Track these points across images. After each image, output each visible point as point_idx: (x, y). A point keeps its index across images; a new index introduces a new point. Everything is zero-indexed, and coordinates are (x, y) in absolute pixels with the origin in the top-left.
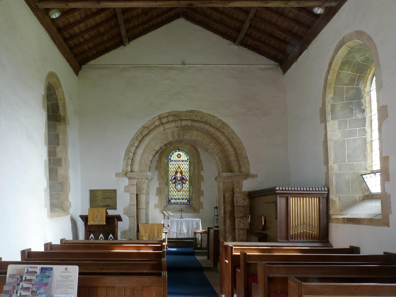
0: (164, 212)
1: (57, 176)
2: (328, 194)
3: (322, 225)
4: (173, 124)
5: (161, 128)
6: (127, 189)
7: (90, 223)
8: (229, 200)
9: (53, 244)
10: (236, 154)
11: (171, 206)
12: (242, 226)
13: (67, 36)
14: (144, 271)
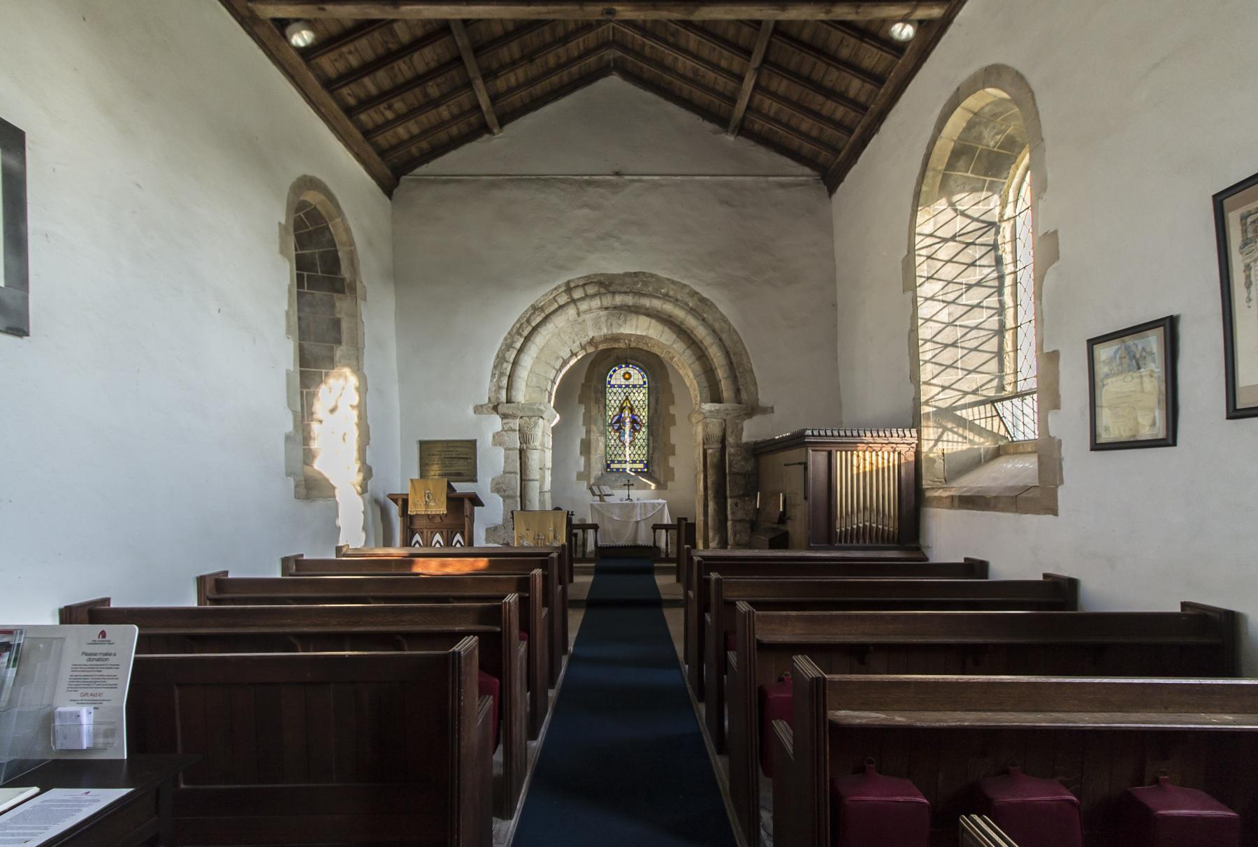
4: (596, 303)
5: (571, 311)
6: (498, 439)
7: (412, 511)
9: (305, 558)
10: (731, 363)
12: (740, 515)
13: (352, 101)
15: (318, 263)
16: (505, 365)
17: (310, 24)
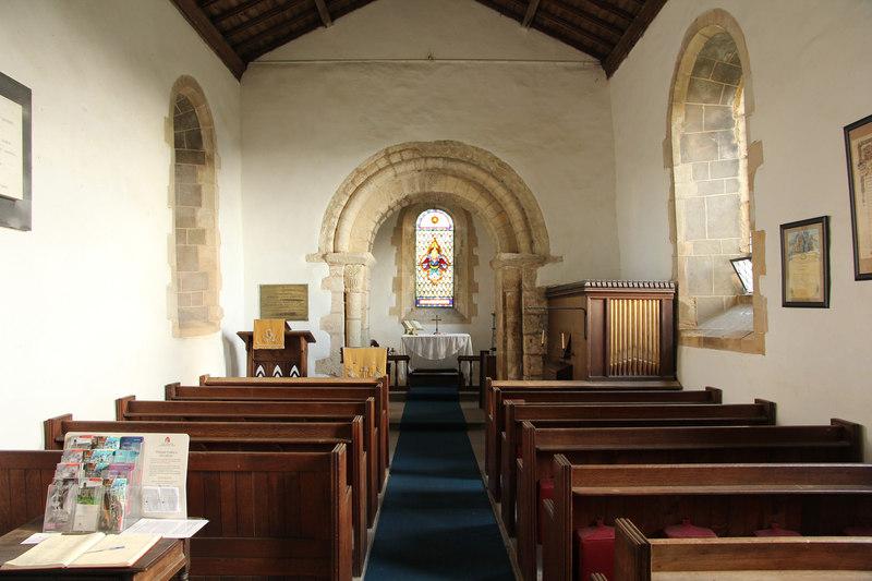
0: (407, 323)
1: (197, 262)
2: (676, 294)
3: (664, 349)
4: (411, 166)
5: (390, 173)
6: (326, 283)
7: (257, 345)
8: (511, 302)
11: (418, 311)
12: (534, 350)
13: (216, 12)
14: (320, 441)
15: (191, 144)
16: (333, 220)
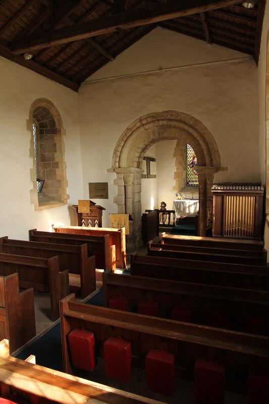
1: (56, 176)
4: (151, 125)
5: (142, 129)
6: (115, 182)
13: (55, 66)
15: (46, 127)
17: (30, 53)
